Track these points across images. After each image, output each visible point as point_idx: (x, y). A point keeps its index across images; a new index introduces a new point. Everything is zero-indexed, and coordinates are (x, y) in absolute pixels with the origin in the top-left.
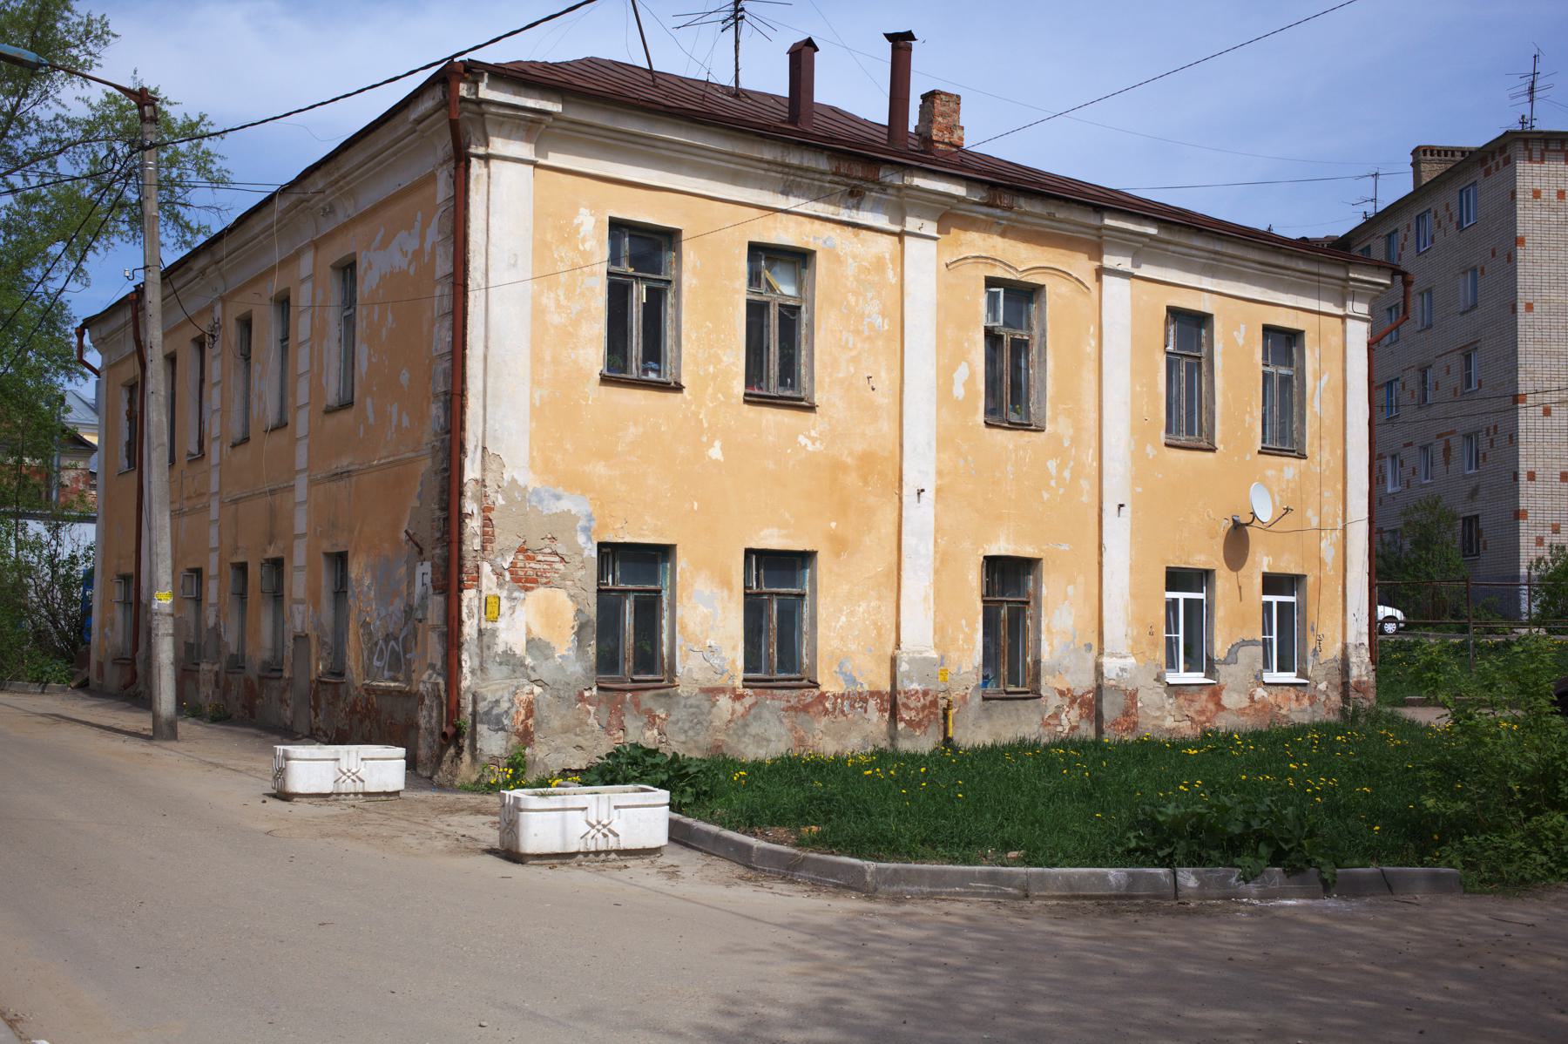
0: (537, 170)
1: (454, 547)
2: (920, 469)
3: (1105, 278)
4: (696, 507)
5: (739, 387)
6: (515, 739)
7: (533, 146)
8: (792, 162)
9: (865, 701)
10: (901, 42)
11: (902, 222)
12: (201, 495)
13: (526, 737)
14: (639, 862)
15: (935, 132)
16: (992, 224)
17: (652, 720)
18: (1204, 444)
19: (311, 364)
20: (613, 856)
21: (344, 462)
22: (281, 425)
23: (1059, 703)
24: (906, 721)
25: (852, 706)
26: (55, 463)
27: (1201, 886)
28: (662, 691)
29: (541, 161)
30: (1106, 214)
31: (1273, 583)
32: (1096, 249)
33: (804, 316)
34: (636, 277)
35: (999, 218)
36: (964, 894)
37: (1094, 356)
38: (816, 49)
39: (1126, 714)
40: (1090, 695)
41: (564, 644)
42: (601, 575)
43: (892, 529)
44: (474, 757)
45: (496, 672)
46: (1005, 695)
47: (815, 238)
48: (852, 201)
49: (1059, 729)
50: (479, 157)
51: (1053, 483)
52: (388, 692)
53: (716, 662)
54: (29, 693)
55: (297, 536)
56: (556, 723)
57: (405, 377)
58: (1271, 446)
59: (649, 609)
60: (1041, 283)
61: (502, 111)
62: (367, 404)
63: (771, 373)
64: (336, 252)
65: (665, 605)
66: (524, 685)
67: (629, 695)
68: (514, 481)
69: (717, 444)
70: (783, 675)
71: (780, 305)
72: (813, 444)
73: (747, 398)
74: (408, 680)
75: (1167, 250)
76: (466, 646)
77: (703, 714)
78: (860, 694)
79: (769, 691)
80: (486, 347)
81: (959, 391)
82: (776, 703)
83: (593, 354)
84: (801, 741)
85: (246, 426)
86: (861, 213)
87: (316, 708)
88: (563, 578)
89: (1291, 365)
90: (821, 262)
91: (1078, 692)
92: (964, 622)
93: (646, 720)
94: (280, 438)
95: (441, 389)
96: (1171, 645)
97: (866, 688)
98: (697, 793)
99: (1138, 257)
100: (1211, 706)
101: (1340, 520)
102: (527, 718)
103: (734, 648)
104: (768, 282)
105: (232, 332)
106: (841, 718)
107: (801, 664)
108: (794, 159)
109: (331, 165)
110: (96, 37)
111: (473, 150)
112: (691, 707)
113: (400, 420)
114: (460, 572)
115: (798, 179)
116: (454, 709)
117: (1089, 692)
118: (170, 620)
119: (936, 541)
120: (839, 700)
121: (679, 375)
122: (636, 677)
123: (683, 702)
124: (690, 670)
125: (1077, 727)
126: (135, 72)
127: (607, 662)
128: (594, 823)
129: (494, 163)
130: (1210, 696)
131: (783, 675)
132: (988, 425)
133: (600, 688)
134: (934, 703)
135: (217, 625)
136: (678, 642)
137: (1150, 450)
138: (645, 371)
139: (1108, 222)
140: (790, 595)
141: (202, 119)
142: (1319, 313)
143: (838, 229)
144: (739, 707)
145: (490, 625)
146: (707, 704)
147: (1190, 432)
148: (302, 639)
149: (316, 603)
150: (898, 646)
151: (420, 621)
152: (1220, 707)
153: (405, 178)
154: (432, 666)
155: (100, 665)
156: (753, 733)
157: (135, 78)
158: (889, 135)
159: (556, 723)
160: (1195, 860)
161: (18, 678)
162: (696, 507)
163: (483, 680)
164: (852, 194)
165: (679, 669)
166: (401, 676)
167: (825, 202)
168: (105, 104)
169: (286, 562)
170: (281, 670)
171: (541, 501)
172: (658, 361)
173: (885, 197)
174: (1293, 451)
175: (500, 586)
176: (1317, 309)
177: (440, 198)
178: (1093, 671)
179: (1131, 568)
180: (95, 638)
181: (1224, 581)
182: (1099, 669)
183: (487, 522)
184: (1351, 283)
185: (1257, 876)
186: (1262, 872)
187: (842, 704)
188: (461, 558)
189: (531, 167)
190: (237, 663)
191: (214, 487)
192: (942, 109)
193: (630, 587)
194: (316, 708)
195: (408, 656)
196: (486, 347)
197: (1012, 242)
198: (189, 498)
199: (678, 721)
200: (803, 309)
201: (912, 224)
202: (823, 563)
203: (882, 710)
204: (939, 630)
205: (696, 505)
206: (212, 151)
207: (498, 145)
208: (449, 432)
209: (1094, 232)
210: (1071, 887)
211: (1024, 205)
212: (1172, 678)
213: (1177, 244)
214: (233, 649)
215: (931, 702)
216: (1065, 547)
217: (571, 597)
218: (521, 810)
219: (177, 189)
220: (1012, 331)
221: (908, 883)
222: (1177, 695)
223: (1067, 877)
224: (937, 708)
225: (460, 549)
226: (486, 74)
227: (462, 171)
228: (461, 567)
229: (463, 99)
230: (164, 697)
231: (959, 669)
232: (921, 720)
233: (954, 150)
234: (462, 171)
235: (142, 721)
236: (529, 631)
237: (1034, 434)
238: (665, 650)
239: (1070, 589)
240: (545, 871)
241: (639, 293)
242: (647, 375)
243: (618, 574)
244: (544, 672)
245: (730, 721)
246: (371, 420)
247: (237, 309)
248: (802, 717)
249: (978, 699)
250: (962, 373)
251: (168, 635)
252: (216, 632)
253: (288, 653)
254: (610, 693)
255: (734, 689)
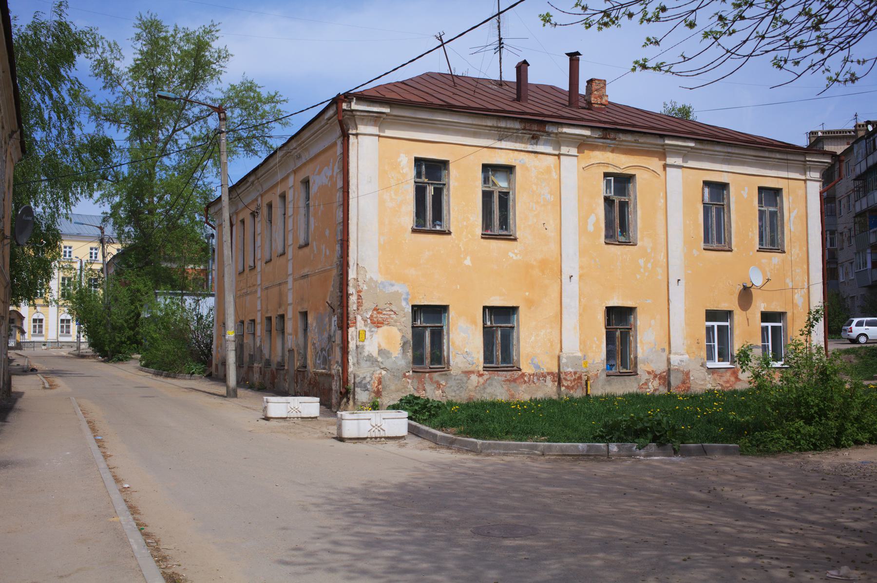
0: (380, 138)
1: (345, 308)
2: (571, 265)
3: (668, 169)
4: (458, 288)
5: (479, 231)
6: (373, 395)
7: (378, 128)
8: (501, 126)
9: (545, 377)
10: (574, 57)
11: (560, 149)
12: (254, 285)
13: (378, 393)
14: (394, 442)
15: (592, 99)
16: (606, 146)
17: (439, 386)
18: (727, 248)
19: (293, 227)
20: (383, 439)
21: (305, 271)
22: (283, 254)
23: (648, 378)
24: (565, 387)
25: (538, 379)
26: (210, 267)
27: (619, 451)
28: (443, 373)
29: (382, 134)
30: (666, 138)
31: (766, 317)
32: (662, 154)
33: (511, 196)
34: (429, 183)
35: (610, 144)
36: (517, 454)
37: (663, 207)
38: (529, 65)
39: (684, 383)
40: (665, 374)
41: (396, 351)
42: (414, 319)
43: (557, 295)
44: (354, 403)
45: (364, 364)
46: (619, 374)
47: (515, 160)
48: (533, 141)
49: (648, 390)
50: (353, 134)
51: (642, 270)
52: (322, 374)
53: (470, 359)
54: (186, 379)
55: (289, 304)
56: (393, 387)
57: (327, 232)
58: (765, 247)
59: (438, 335)
60: (634, 173)
61: (362, 114)
62: (314, 244)
63: (495, 223)
64: (302, 176)
65: (445, 333)
66: (377, 370)
67: (427, 375)
68: (371, 278)
69: (468, 258)
70: (504, 365)
71: (499, 192)
72: (516, 256)
73: (483, 236)
74: (330, 369)
75: (701, 153)
76: (350, 353)
77: (463, 383)
78: (542, 373)
79: (496, 372)
80: (358, 219)
81: (591, 228)
82: (500, 378)
83: (408, 218)
84: (512, 396)
85: (271, 256)
86: (538, 146)
87: (297, 383)
88: (396, 321)
89: (776, 206)
90: (518, 170)
91: (658, 372)
92: (596, 339)
93: (435, 386)
94: (282, 259)
95: (339, 238)
96: (710, 349)
97: (545, 370)
98: (430, 415)
99: (685, 157)
100: (733, 379)
101: (806, 284)
102: (379, 385)
103: (478, 352)
104: (493, 181)
105: (265, 210)
106: (533, 385)
107: (513, 360)
108: (503, 124)
109: (298, 137)
110: (224, 57)
111: (350, 132)
112: (457, 380)
113: (326, 252)
114: (348, 320)
115: (506, 133)
116: (346, 381)
117: (664, 372)
118: (233, 344)
119: (580, 300)
120: (532, 377)
121: (450, 227)
122: (431, 366)
123: (454, 378)
124: (457, 363)
125: (657, 389)
126: (244, 73)
127: (418, 360)
128: (374, 425)
129: (359, 137)
130: (731, 374)
131: (504, 365)
132: (606, 243)
133: (413, 372)
134: (580, 378)
135: (260, 345)
136: (451, 350)
137: (695, 252)
138: (434, 226)
139: (667, 142)
140: (507, 327)
141: (276, 94)
142: (788, 179)
143: (526, 154)
144: (481, 380)
145: (361, 344)
146: (465, 379)
147: (719, 241)
148: (291, 351)
149: (296, 335)
150: (561, 351)
151: (334, 342)
152: (737, 379)
153: (326, 143)
154: (337, 362)
155: (217, 365)
156: (488, 392)
157: (243, 77)
158: (569, 101)
159: (393, 387)
160: (620, 440)
161: (180, 372)
162: (458, 288)
163: (359, 368)
164: (533, 138)
165: (451, 362)
166: (327, 367)
167: (519, 143)
168: (230, 90)
169: (285, 316)
170: (284, 366)
171: (384, 287)
172: (440, 220)
173: (549, 138)
174: (779, 249)
175: (365, 325)
176: (787, 177)
177: (338, 153)
178: (666, 362)
179: (686, 311)
180: (214, 353)
181: (739, 316)
182: (669, 360)
183: (359, 297)
184: (808, 163)
185: (644, 447)
186: (647, 445)
187: (533, 378)
188: (348, 313)
189: (377, 137)
190: (268, 363)
191: (259, 282)
192: (596, 87)
193: (428, 325)
194: (297, 383)
195: (330, 358)
196: (358, 219)
197: (618, 155)
198: (250, 287)
199: (451, 386)
200: (511, 193)
201: (564, 150)
202: (522, 312)
203: (554, 381)
204: (582, 342)
205: (458, 286)
206: (282, 110)
207: (362, 129)
208: (342, 258)
209: (660, 147)
210: (562, 451)
211: (622, 137)
212: (710, 365)
213: (706, 150)
214: (267, 356)
215: (578, 377)
216: (649, 301)
217: (400, 330)
218: (343, 420)
219: (266, 130)
220: (619, 197)
221: (494, 448)
222: (713, 373)
223: (561, 447)
224: (581, 380)
225: (347, 310)
226: (355, 98)
227: (346, 141)
228: (348, 317)
229: (345, 110)
230: (231, 378)
231: (593, 361)
232: (573, 386)
233: (603, 107)
234: (346, 141)
235: (223, 390)
236: (379, 346)
237: (631, 247)
238: (445, 354)
239: (653, 322)
240: (351, 445)
241: (430, 191)
242: (436, 227)
243: (422, 319)
244: (387, 364)
245: (477, 387)
246: (315, 252)
247: (266, 200)
248: (513, 384)
249: (604, 376)
250: (592, 219)
251: (233, 350)
252: (260, 349)
253: (286, 358)
254: (418, 374)
255: (479, 371)
